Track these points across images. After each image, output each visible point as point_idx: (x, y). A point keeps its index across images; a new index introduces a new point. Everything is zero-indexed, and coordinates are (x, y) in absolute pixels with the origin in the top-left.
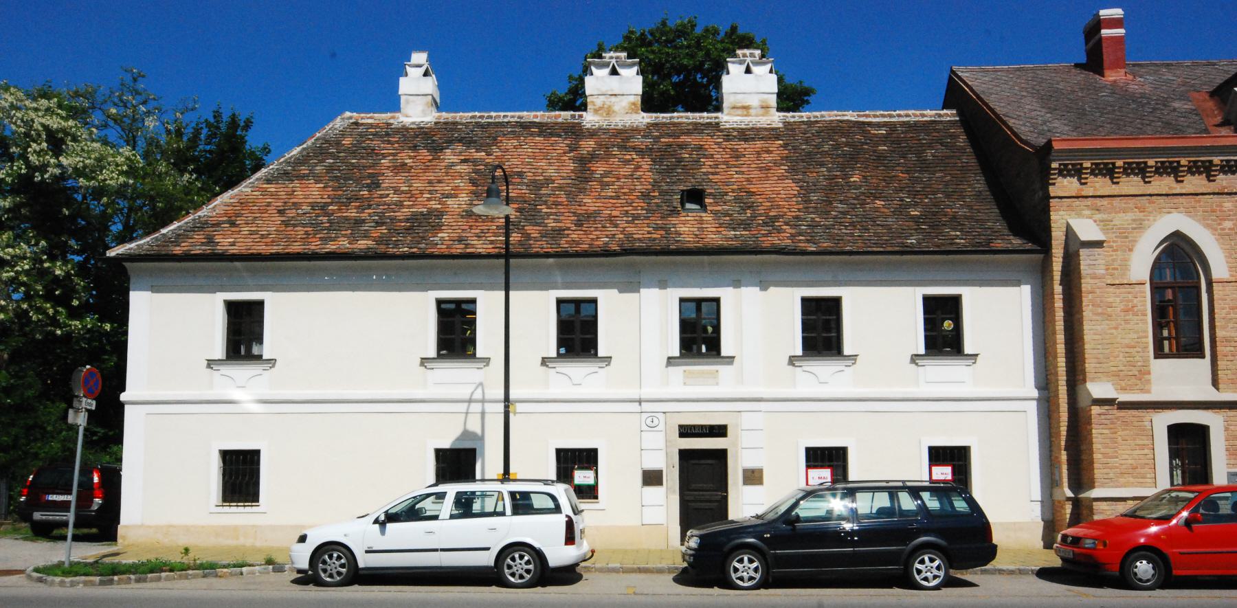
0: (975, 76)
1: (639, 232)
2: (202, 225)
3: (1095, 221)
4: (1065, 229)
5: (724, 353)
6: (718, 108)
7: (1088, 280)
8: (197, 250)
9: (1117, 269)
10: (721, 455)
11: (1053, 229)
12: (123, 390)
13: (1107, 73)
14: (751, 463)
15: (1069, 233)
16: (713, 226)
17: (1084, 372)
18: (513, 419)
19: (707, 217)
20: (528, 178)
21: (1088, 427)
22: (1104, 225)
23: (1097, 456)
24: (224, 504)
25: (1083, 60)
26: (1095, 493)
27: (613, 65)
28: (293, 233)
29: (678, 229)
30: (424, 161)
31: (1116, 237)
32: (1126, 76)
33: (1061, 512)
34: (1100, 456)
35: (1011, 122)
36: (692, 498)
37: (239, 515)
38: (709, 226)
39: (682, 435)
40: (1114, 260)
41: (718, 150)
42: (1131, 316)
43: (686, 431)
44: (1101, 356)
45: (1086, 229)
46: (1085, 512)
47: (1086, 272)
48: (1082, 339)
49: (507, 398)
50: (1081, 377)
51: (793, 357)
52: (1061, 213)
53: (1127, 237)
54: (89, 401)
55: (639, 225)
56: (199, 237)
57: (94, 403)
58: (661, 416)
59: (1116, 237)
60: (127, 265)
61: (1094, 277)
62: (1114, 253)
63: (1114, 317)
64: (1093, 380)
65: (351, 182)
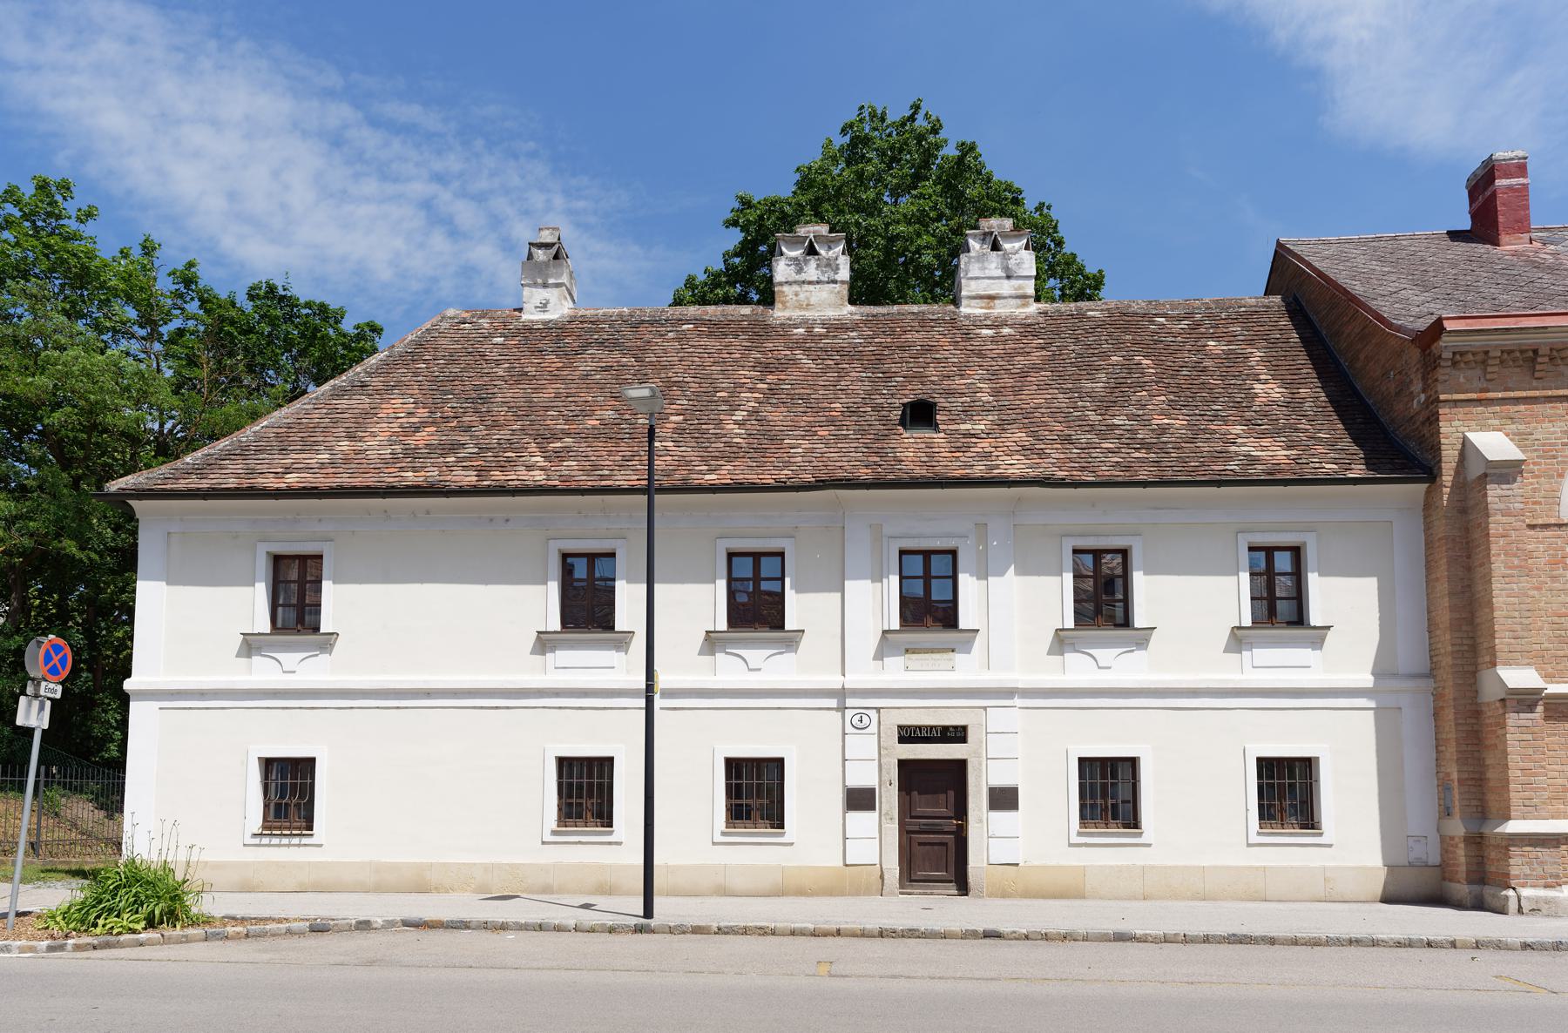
0: (1313, 250)
1: (844, 459)
2: (243, 452)
3: (1507, 435)
4: (1459, 447)
5: (962, 625)
6: (956, 302)
7: (1499, 517)
8: (232, 483)
9: (1540, 503)
10: (960, 766)
11: (1443, 447)
12: (128, 674)
13: (1504, 238)
14: (1000, 779)
15: (1466, 449)
16: (947, 450)
17: (1492, 651)
18: (997, 835)
19: (938, 438)
20: (692, 390)
21: (1500, 732)
22: (1520, 439)
23: (1514, 773)
24: (264, 832)
25: (1465, 223)
26: (1514, 827)
27: (811, 240)
28: (365, 461)
29: (898, 454)
30: (551, 369)
31: (1537, 457)
32: (1531, 243)
33: (1455, 852)
34: (1519, 773)
35: (1373, 304)
36: (916, 828)
37: (286, 853)
38: (943, 450)
39: (902, 740)
40: (1534, 490)
41: (954, 352)
42: (1561, 571)
43: (909, 735)
44: (1518, 627)
45: (1494, 444)
46: (1493, 855)
47: (1495, 506)
48: (1490, 604)
49: (650, 688)
50: (1487, 659)
51: (1061, 630)
52: (1456, 423)
53: (1554, 457)
54: (51, 686)
55: (843, 450)
56: (237, 466)
57: (59, 688)
58: (873, 714)
59: (1537, 457)
60: (133, 503)
61: (1507, 513)
62: (1535, 480)
63: (1535, 572)
64: (1507, 663)
65: (450, 396)
